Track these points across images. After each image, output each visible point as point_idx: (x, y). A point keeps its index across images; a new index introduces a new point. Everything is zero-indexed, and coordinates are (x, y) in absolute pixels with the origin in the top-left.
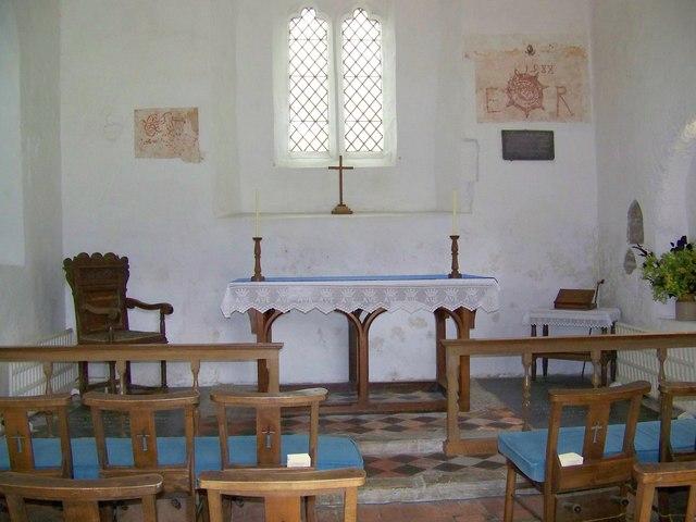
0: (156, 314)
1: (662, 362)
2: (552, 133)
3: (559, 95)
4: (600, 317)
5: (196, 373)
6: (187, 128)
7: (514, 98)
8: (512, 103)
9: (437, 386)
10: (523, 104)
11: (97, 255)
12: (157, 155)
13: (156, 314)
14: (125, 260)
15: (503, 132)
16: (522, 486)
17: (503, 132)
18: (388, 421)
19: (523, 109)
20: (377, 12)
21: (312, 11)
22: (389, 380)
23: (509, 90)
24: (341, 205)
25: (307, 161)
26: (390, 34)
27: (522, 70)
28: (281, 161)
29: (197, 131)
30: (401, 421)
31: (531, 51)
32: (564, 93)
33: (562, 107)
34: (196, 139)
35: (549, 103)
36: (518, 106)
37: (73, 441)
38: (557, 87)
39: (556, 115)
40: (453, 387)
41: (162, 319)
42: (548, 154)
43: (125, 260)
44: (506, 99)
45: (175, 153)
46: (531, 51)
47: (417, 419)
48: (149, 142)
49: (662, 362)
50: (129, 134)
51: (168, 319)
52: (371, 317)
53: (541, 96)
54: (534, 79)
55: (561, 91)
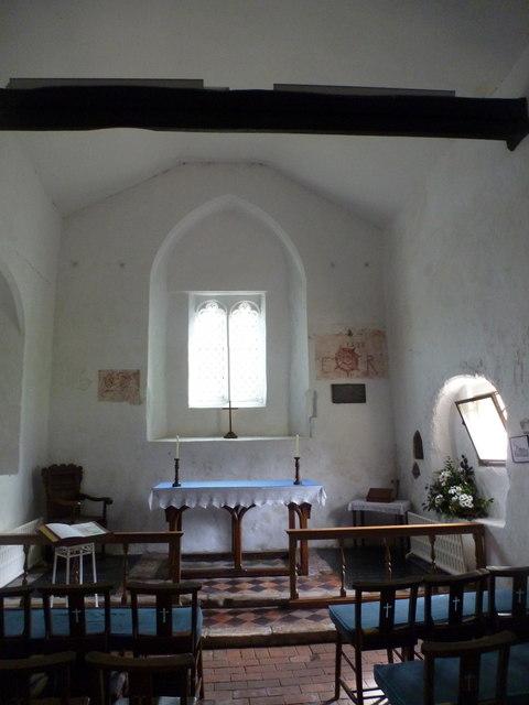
1: (433, 543)
2: (365, 401)
4: (399, 506)
5: (126, 549)
6: (132, 383)
9: (286, 556)
12: (112, 399)
14: (81, 468)
15: (333, 386)
16: (350, 693)
17: (333, 386)
18: (252, 582)
22: (259, 550)
23: (337, 359)
27: (345, 346)
30: (262, 582)
31: (350, 334)
33: (371, 369)
39: (366, 374)
40: (298, 559)
42: (363, 400)
44: (334, 364)
45: (124, 398)
47: (273, 581)
49: (433, 543)
50: (95, 387)
51: (109, 507)
52: (245, 510)
53: (357, 363)
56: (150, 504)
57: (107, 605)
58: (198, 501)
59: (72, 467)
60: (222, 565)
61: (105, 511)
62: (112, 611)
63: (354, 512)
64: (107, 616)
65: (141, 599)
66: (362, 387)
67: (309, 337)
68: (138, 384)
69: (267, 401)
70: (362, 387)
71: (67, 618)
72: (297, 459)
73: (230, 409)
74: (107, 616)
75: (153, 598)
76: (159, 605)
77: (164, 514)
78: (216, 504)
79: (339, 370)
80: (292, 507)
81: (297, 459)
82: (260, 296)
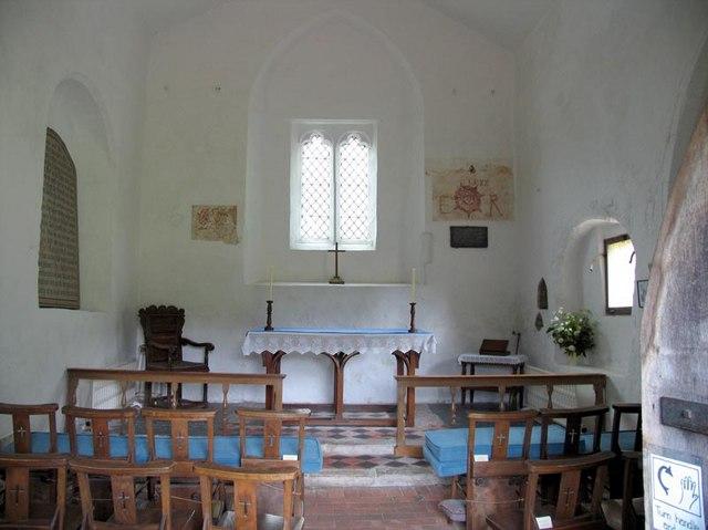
8: (459, 207)
10: (466, 207)
15: (452, 228)
17: (452, 228)
24: (337, 277)
27: (467, 184)
31: (472, 170)
35: (485, 207)
39: (490, 215)
43: (182, 311)
46: (472, 170)
59: (173, 309)
66: (485, 229)
79: (458, 210)
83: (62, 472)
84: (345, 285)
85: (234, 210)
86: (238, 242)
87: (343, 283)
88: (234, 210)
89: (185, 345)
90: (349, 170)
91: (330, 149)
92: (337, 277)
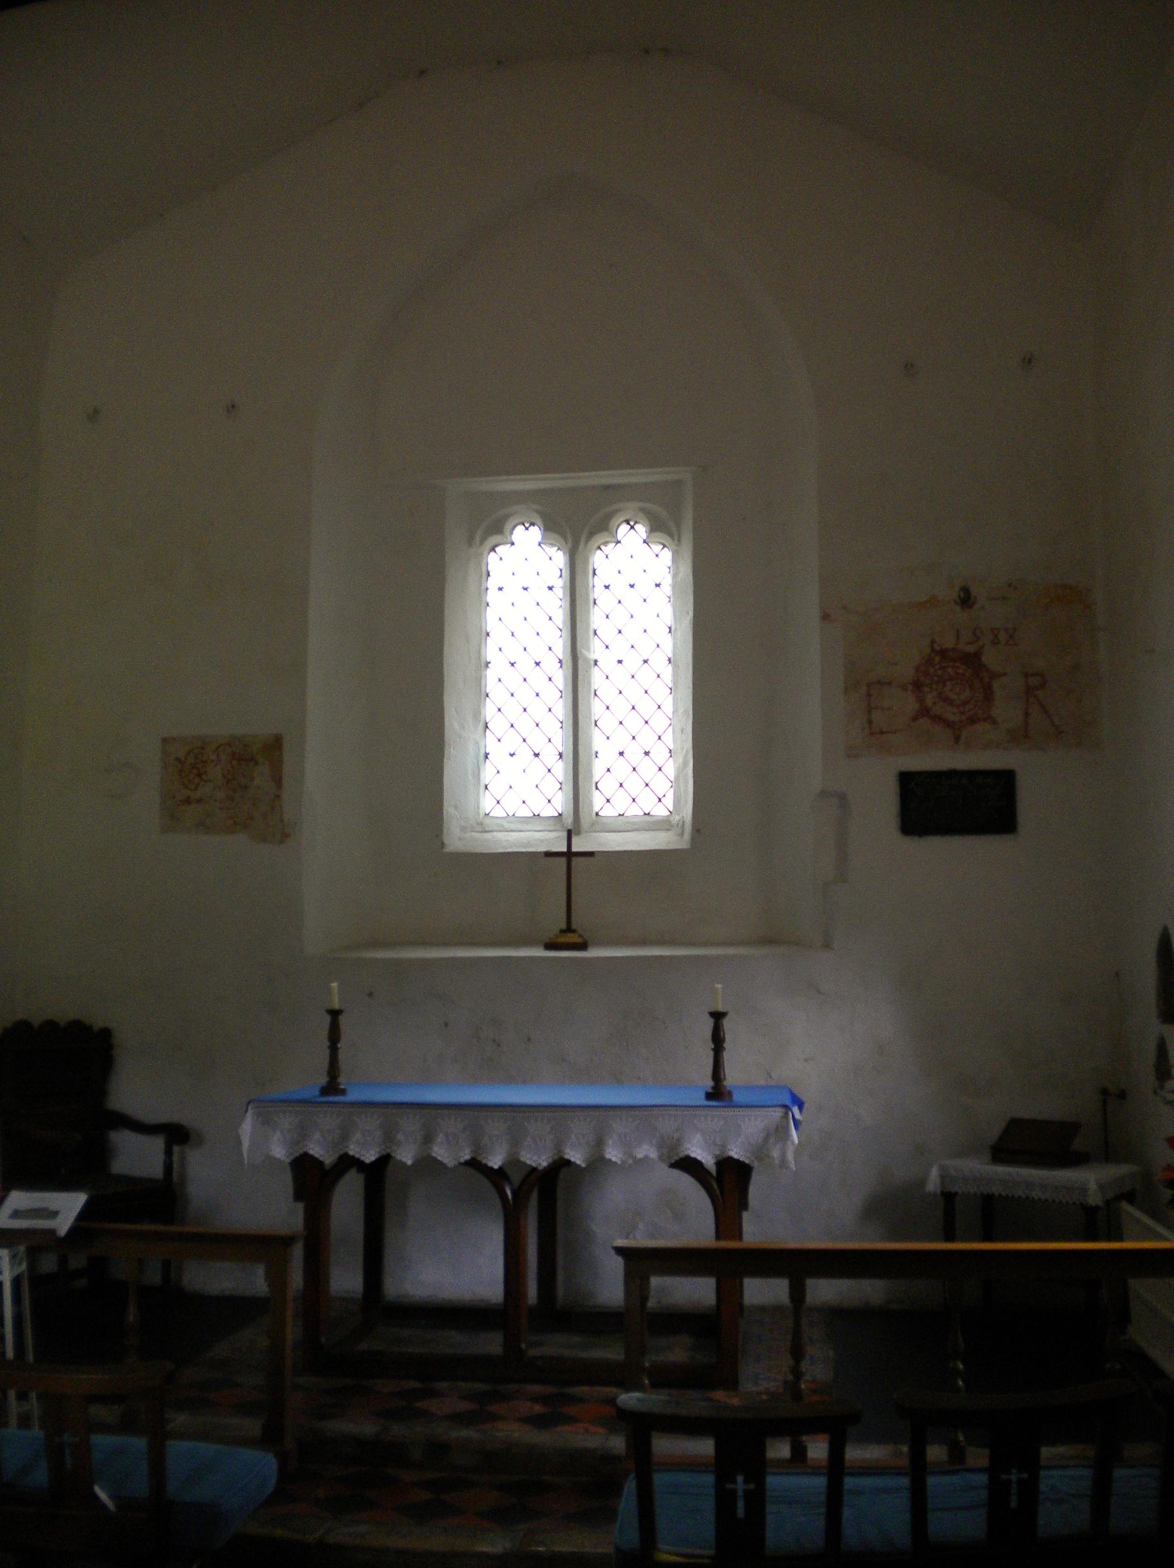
0: (157, 1144)
3: (1029, 691)
7: (929, 701)
8: (924, 712)
10: (952, 715)
11: (50, 1025)
13: (157, 1144)
14: (106, 1033)
15: (906, 779)
17: (906, 779)
19: (948, 724)
20: (661, 528)
21: (639, 527)
23: (917, 686)
24: (569, 929)
25: (514, 836)
26: (686, 569)
27: (949, 642)
28: (457, 838)
29: (279, 785)
31: (966, 600)
32: (1043, 686)
34: (278, 797)
35: (1006, 711)
36: (937, 719)
37: (810, 1282)
38: (1026, 675)
39: (1021, 736)
41: (169, 1153)
43: (106, 1033)
44: (911, 704)
46: (966, 600)
48: (188, 801)
54: (973, 660)
55: (1034, 681)
56: (246, 1143)
57: (836, 1467)
58: (428, 1139)
59: (78, 1028)
60: (491, 1344)
61: (168, 1167)
62: (849, 1482)
63: (949, 1197)
64: (835, 1498)
65: (664, 1445)
66: (1005, 780)
67: (825, 617)
68: (278, 780)
69: (697, 830)
70: (1005, 780)
71: (708, 1506)
72: (335, 1014)
73: (569, 855)
74: (835, 1498)
75: (705, 1447)
76: (723, 1467)
77: (288, 1178)
78: (441, 1152)
79: (925, 723)
80: (303, 1166)
81: (335, 1014)
82: (679, 483)
83: (981, 643)
84: (592, 953)
85: (274, 746)
86: (286, 836)
87: (583, 946)
88: (274, 746)
89: (571, 850)
90: (620, 617)
91: (559, 558)
92: (569, 929)
